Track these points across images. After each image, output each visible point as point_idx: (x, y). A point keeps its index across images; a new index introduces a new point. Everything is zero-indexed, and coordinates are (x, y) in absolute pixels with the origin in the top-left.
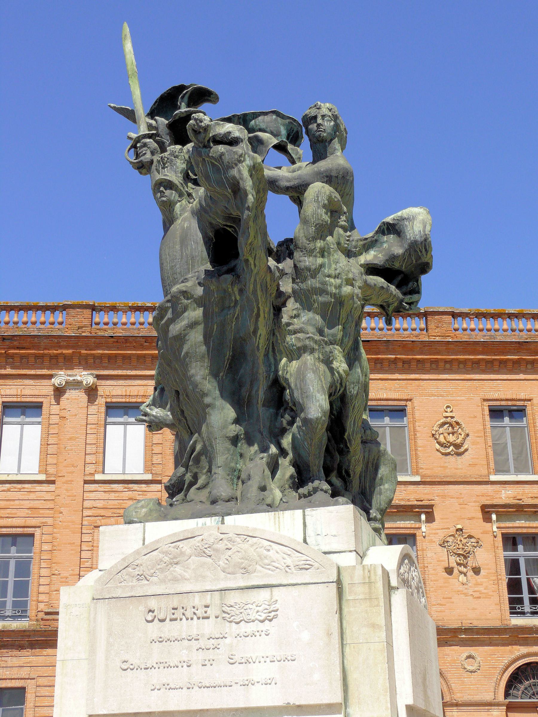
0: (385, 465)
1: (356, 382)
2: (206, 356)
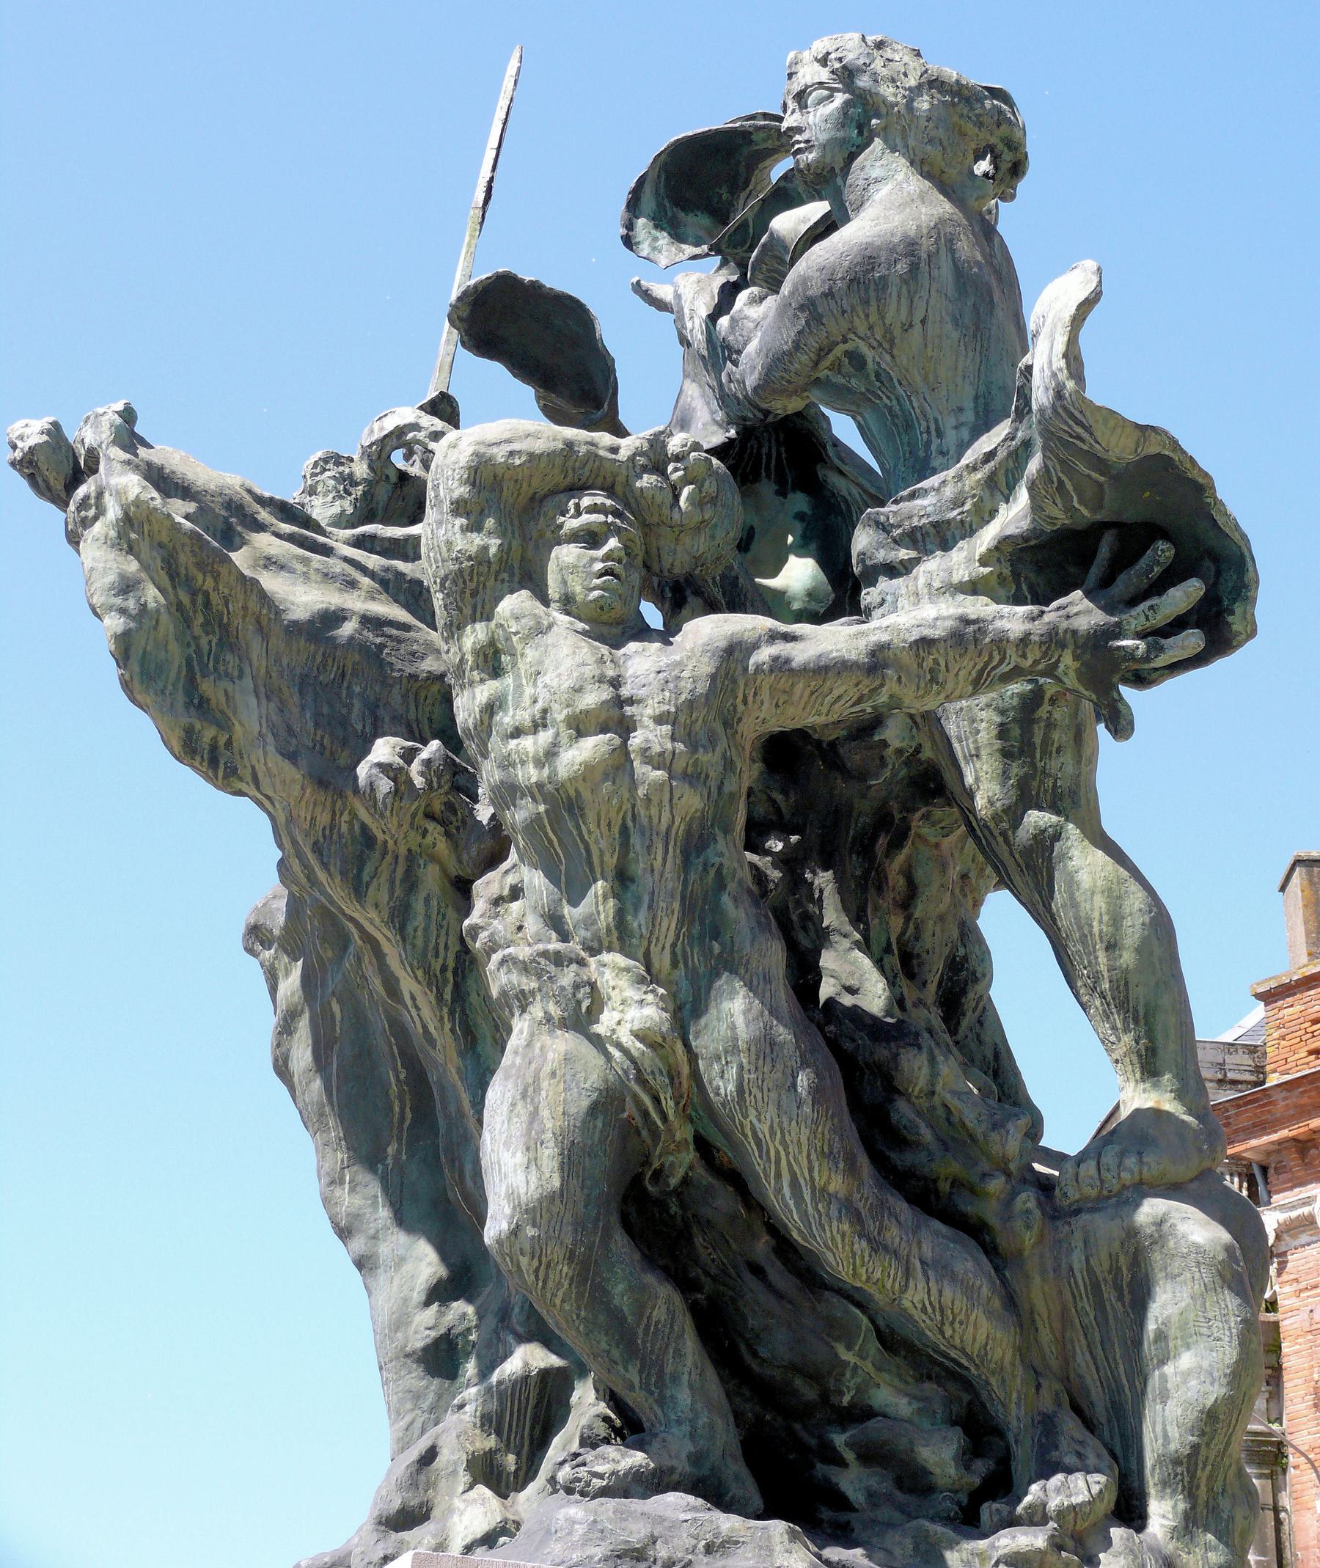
0: (1174, 1277)
1: (726, 1052)
2: (327, 1109)
